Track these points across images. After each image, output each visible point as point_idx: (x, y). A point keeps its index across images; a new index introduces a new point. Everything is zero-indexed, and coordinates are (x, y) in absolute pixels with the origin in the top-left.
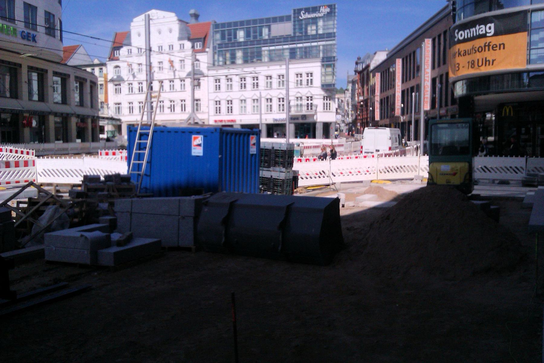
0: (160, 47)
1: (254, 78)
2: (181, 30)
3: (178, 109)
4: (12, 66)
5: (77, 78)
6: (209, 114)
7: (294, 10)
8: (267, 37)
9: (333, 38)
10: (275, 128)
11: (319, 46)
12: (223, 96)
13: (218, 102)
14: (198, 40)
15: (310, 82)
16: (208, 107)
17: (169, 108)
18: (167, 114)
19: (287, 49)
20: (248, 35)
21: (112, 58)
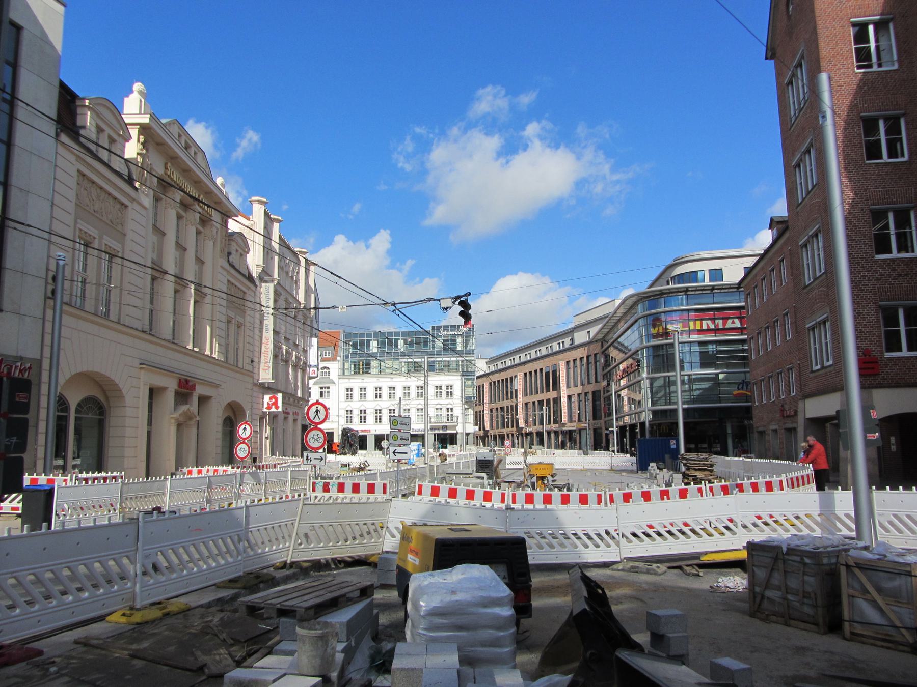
7: (433, 327)
11: (458, 361)
15: (450, 394)
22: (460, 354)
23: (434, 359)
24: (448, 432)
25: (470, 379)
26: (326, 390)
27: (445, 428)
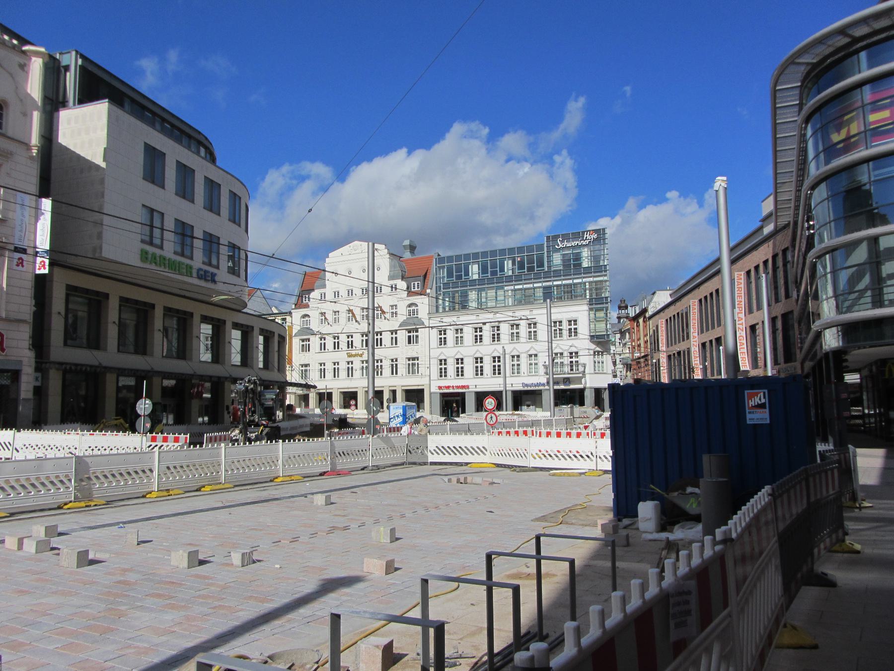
0: (337, 294)
1: (476, 329)
2: (392, 267)
5: (263, 332)
6: (430, 378)
7: (548, 238)
8: (510, 273)
9: (603, 273)
10: (524, 397)
11: (585, 283)
12: (450, 352)
14: (415, 278)
15: (573, 333)
16: (429, 368)
18: (386, 378)
19: (539, 287)
20: (484, 269)
21: (299, 305)
22: (588, 270)
23: (551, 283)
24: (572, 387)
25: (601, 309)
26: (415, 334)
27: (567, 381)
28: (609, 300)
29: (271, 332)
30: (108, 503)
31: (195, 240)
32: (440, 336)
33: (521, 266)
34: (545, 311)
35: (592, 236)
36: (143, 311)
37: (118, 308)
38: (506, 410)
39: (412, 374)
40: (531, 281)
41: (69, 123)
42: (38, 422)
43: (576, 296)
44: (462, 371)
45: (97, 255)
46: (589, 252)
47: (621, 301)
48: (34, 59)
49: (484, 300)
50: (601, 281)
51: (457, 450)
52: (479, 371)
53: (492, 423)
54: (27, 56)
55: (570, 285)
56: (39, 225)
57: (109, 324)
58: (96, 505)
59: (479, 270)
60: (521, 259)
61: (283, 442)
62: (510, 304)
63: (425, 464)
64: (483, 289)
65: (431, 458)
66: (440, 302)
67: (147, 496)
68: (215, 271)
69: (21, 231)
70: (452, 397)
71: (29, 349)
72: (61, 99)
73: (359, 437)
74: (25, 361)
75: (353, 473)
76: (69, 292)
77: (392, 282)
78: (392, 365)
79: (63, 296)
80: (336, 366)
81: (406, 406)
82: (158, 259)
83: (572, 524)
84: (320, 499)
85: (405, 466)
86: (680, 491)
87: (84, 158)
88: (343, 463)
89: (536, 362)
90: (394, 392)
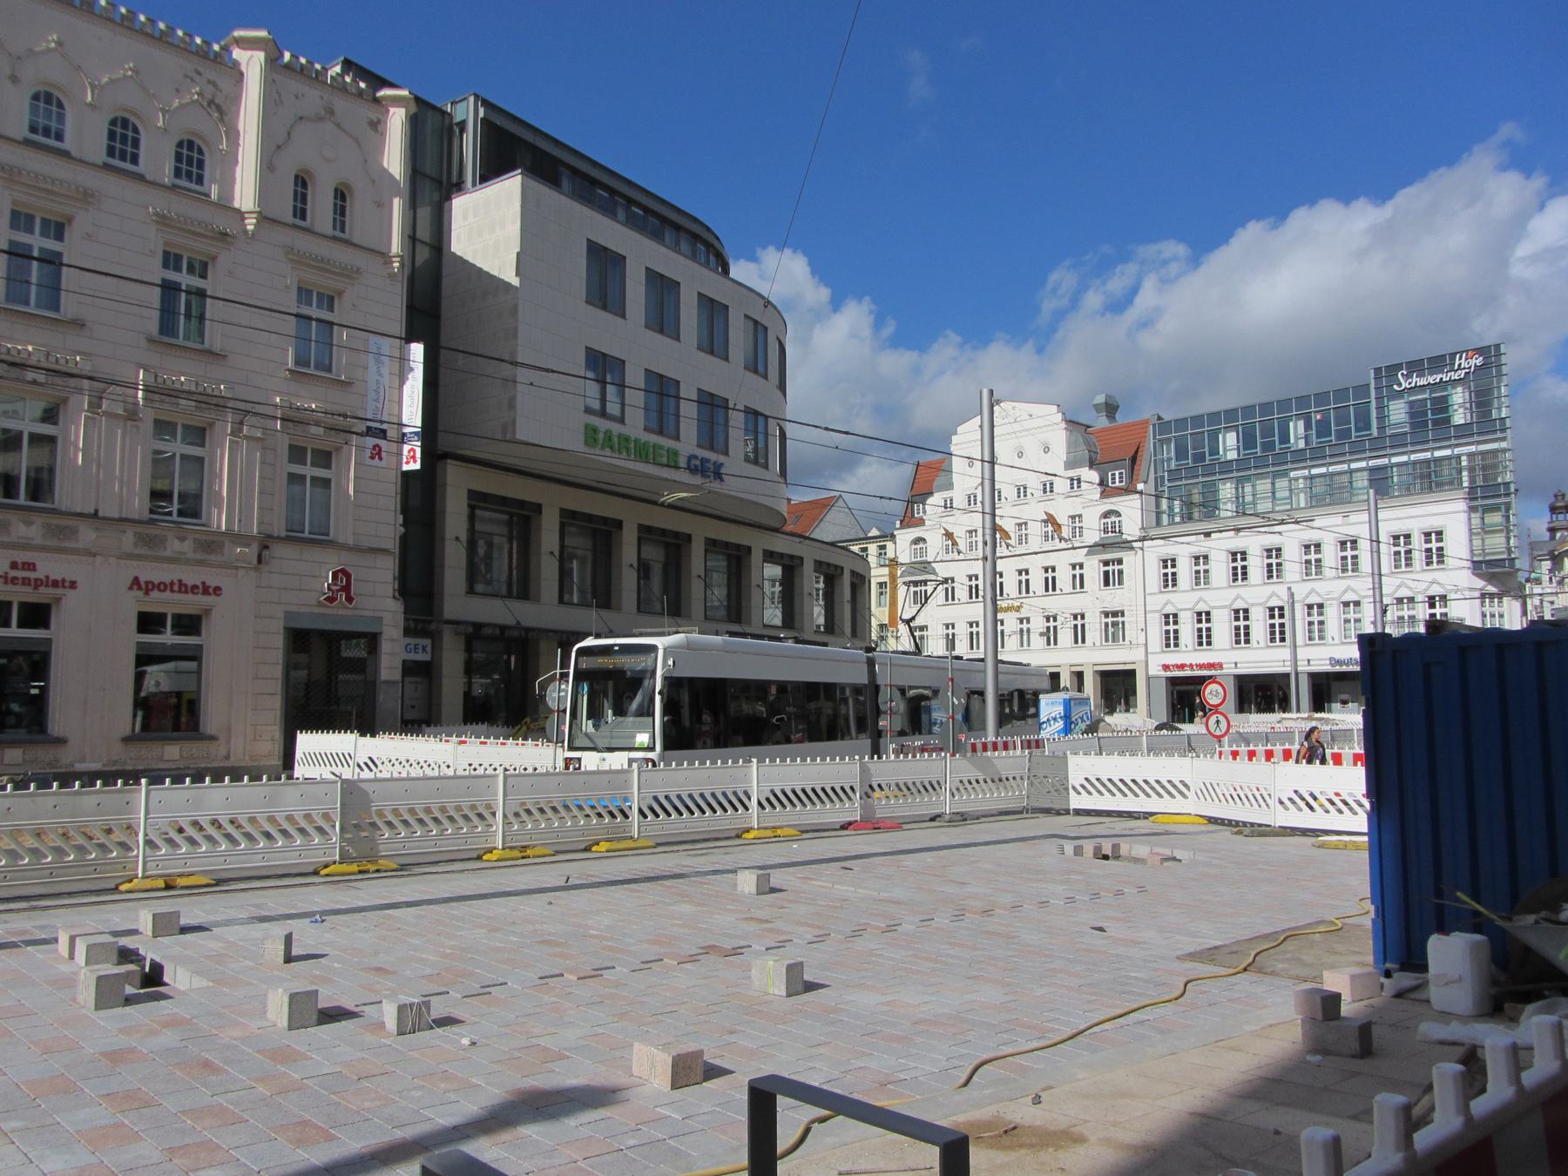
3: (1066, 636)
4: (598, 526)
5: (819, 565)
6: (1146, 649)
7: (1378, 370)
8: (1301, 444)
9: (1499, 435)
10: (1335, 686)
11: (1459, 457)
12: (1184, 600)
13: (1171, 618)
14: (1114, 463)
15: (1436, 557)
16: (1145, 630)
17: (1042, 634)
20: (1247, 441)
21: (909, 520)
22: (1464, 432)
23: (1385, 461)
28: (1512, 490)
29: (836, 567)
30: (403, 867)
31: (683, 403)
32: (1165, 571)
33: (1323, 430)
34: (1365, 517)
35: (1473, 362)
36: (603, 533)
37: (557, 527)
38: (1298, 710)
39: (1114, 641)
40: (1342, 459)
41: (465, 218)
42: (418, 721)
43: (1439, 485)
44: (1209, 636)
45: (508, 437)
46: (1467, 394)
47: (1556, 496)
48: (392, 110)
49: (1249, 499)
50: (1494, 452)
51: (1152, 788)
52: (1242, 636)
53: (1218, 733)
54: (383, 106)
55: (1427, 462)
56: (406, 389)
57: (624, 568)
58: (378, 871)
59: (1238, 442)
60: (1323, 417)
61: (758, 762)
62: (1302, 505)
63: (1067, 812)
64: (1248, 479)
65: (1076, 802)
66: (1164, 504)
67: (594, 849)
68: (722, 459)
69: (377, 400)
70: (1192, 684)
71: (394, 597)
72: (454, 180)
73: (914, 756)
74: (387, 618)
75: (905, 826)
76: (475, 503)
77: (1073, 473)
78: (1076, 626)
79: (465, 510)
80: (974, 630)
81: (1070, 700)
82: (616, 440)
83: (1272, 973)
84: (747, 882)
85: (1025, 815)
86: (1543, 914)
87: (487, 273)
88: (886, 806)
89: (1358, 616)
90: (1079, 676)
